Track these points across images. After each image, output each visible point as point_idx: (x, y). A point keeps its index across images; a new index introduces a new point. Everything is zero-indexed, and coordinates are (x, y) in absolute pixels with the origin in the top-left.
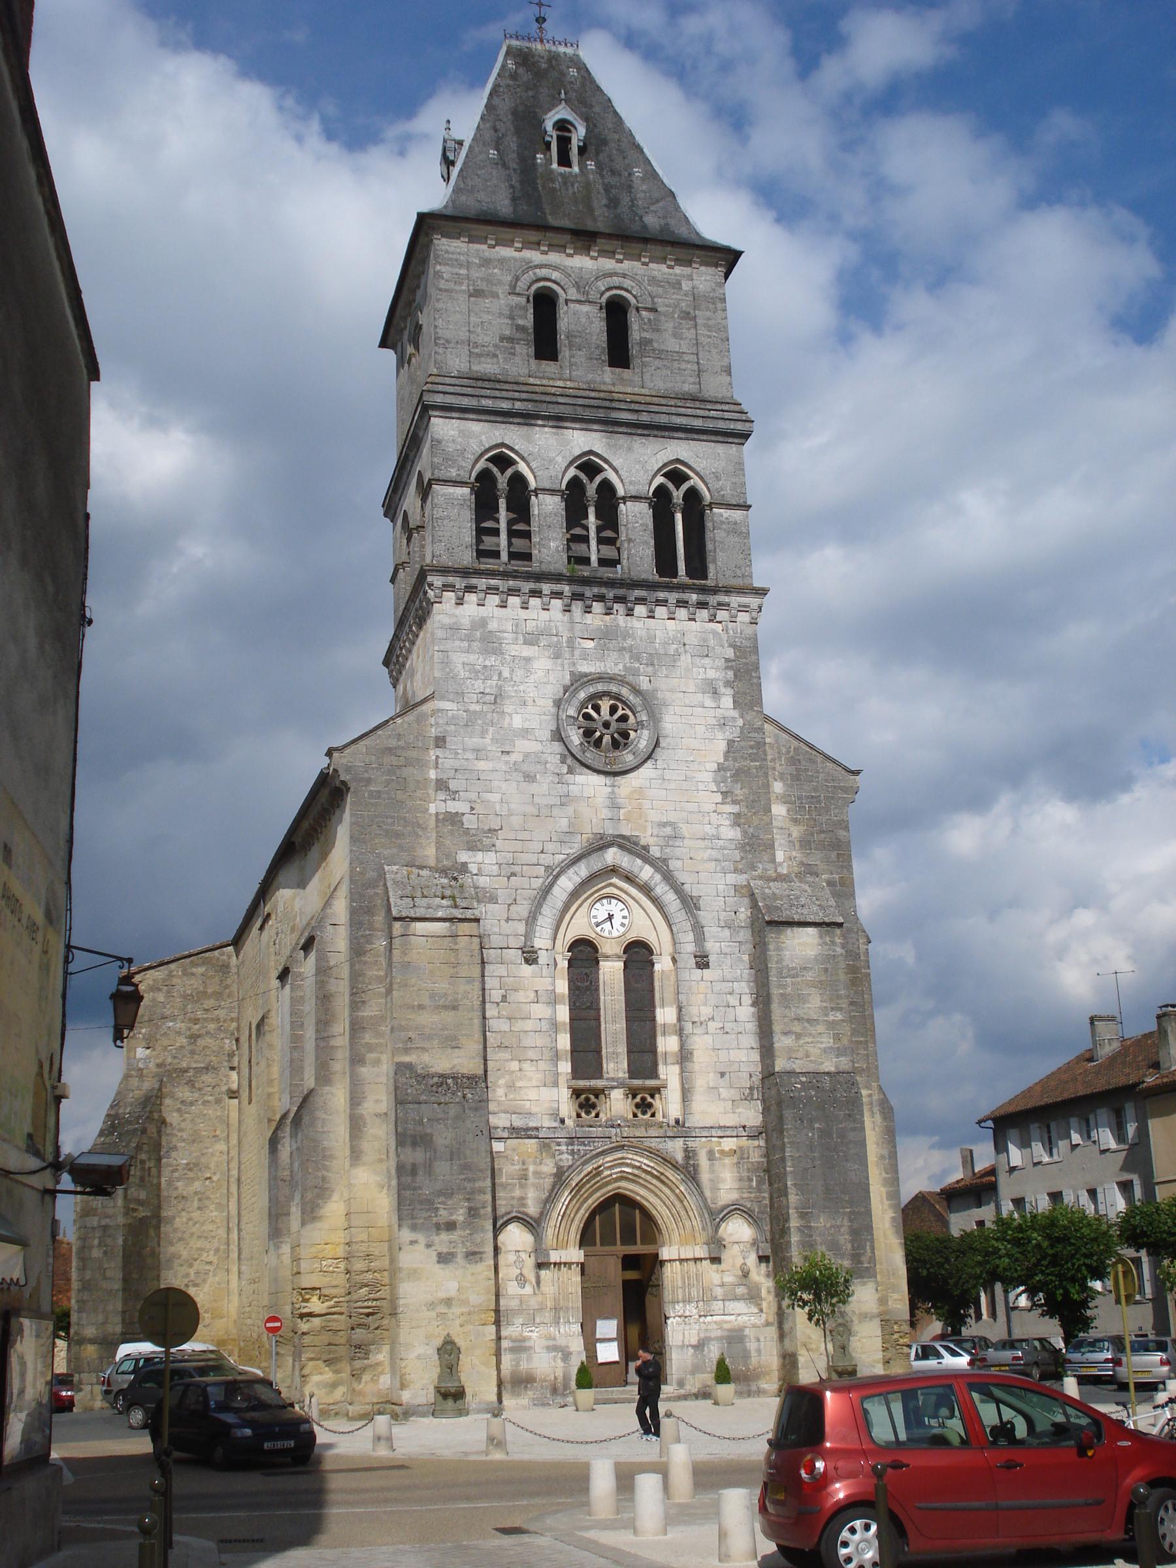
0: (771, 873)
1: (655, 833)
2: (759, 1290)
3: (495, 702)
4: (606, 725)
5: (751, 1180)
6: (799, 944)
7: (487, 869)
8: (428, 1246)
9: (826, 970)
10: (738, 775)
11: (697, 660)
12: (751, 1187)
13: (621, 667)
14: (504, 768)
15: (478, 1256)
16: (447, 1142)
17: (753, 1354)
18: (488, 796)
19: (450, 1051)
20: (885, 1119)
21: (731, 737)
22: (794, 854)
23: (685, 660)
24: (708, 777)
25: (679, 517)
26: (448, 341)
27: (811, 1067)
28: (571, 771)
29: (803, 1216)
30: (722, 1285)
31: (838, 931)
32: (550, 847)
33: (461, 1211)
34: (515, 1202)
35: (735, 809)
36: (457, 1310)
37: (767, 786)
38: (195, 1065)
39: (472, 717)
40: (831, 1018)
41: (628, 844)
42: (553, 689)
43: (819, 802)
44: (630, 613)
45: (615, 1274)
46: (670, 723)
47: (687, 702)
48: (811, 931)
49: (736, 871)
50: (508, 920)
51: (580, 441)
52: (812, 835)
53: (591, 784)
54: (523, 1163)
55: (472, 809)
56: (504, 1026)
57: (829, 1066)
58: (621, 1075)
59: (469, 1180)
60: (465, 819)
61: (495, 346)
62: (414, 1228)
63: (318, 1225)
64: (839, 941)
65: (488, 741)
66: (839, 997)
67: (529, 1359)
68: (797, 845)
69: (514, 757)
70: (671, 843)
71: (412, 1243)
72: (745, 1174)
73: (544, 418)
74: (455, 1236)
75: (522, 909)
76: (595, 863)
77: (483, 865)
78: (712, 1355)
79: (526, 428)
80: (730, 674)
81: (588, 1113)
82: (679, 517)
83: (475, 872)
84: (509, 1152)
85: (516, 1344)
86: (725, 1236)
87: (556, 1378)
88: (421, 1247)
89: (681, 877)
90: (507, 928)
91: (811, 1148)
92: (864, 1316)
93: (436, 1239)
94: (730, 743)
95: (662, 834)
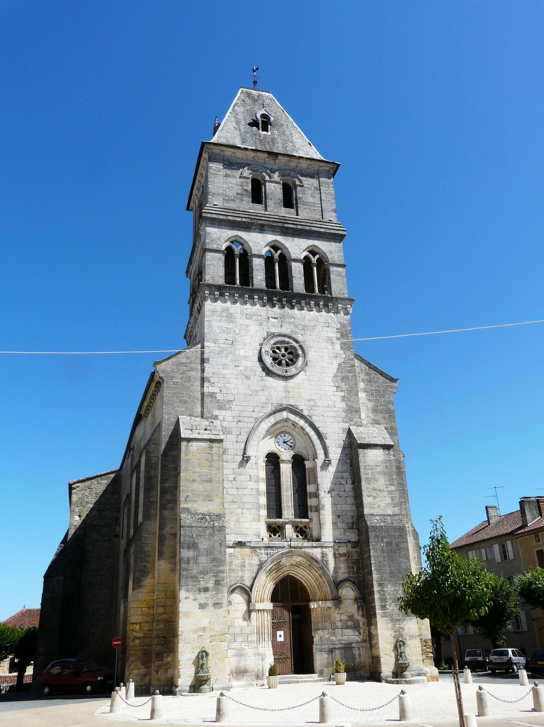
2: (359, 623)
5: (353, 568)
6: (374, 454)
7: (227, 419)
8: (195, 600)
9: (387, 466)
10: (343, 379)
12: (353, 571)
13: (289, 330)
14: (236, 373)
15: (220, 605)
16: (205, 547)
17: (357, 657)
23: (319, 328)
24: (330, 379)
29: (380, 585)
30: (341, 621)
32: (257, 409)
33: (212, 582)
34: (239, 579)
35: (342, 394)
36: (208, 634)
37: (356, 384)
38: (100, 524)
40: (390, 489)
42: (259, 339)
43: (380, 392)
49: (343, 422)
51: (271, 237)
52: (377, 406)
55: (221, 391)
56: (234, 491)
57: (390, 512)
59: (215, 566)
61: (235, 197)
62: (187, 590)
63: (141, 590)
65: (228, 360)
66: (393, 479)
68: (371, 411)
69: (240, 368)
71: (186, 598)
72: (351, 565)
74: (208, 595)
78: (337, 657)
80: (339, 335)
81: (275, 535)
84: (236, 554)
86: (341, 596)
87: (258, 670)
88: (191, 600)
89: (317, 424)
91: (383, 551)
92: (412, 637)
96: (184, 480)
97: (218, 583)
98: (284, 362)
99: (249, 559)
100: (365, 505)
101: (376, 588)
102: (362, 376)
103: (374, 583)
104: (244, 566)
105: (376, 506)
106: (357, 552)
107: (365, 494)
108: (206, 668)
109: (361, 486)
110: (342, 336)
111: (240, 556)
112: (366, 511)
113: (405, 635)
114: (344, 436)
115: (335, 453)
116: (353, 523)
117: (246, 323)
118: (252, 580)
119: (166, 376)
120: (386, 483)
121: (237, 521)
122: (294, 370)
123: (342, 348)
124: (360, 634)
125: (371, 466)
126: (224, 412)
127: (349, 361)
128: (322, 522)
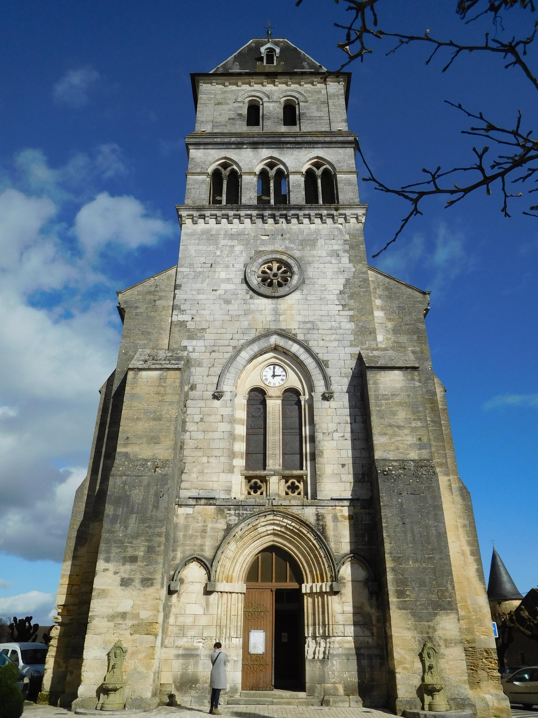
0: (374, 346)
1: (301, 327)
3: (211, 266)
4: (275, 275)
6: (390, 380)
7: (197, 349)
8: (116, 573)
10: (352, 296)
11: (328, 241)
13: (283, 247)
14: (213, 298)
15: (150, 582)
18: (203, 312)
19: (153, 445)
20: (464, 500)
21: (348, 277)
22: (389, 336)
23: (321, 242)
25: (319, 181)
26: (202, 122)
27: (401, 457)
28: (251, 298)
29: (396, 560)
31: (416, 373)
32: (237, 336)
33: (143, 549)
34: (196, 548)
35: (351, 313)
37: (370, 301)
39: (197, 275)
40: (414, 425)
41: (283, 334)
42: (243, 259)
44: (288, 222)
45: (268, 602)
46: (311, 272)
47: (321, 261)
48: (397, 372)
50: (208, 376)
51: (266, 153)
52: (401, 326)
53: (263, 304)
54: (205, 522)
55: (193, 318)
56: (200, 435)
57: (414, 455)
58: (277, 467)
59: (149, 527)
60: (188, 324)
62: (107, 560)
64: (416, 378)
65: (205, 285)
66: (419, 412)
67: (196, 664)
69: (218, 293)
70: (310, 332)
73: (247, 143)
74: (134, 567)
75: (217, 370)
76: (262, 344)
77: (196, 348)
79: (238, 150)
80: (347, 247)
81: (255, 492)
82: (319, 181)
83: (191, 350)
84: (196, 514)
85: (188, 652)
88: (110, 574)
89: (316, 350)
90: (207, 380)
92: (448, 643)
93: (122, 568)
94: (347, 280)
95: (305, 327)
96: (126, 419)
97: (150, 550)
98: (275, 281)
99: (212, 522)
100: (375, 448)
101: (389, 564)
102: (379, 292)
103: (386, 556)
104: (204, 531)
105: (392, 448)
106: (369, 513)
107: (376, 430)
108: (118, 673)
109: (370, 422)
110: (352, 247)
111: (200, 518)
112: (378, 455)
113: (437, 639)
114: (353, 363)
115: (341, 385)
116: (363, 474)
117: (230, 244)
118: (215, 551)
119: (127, 307)
120: (409, 416)
121: (201, 472)
122: (288, 289)
123: (350, 261)
124: (373, 634)
125: (386, 395)
126: (194, 342)
127: (361, 275)
128: (318, 473)
